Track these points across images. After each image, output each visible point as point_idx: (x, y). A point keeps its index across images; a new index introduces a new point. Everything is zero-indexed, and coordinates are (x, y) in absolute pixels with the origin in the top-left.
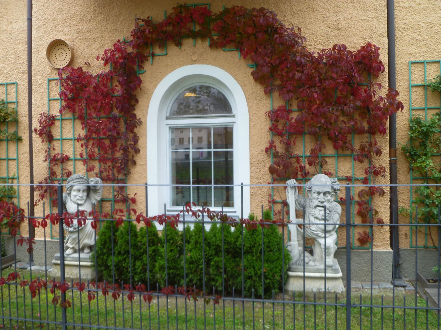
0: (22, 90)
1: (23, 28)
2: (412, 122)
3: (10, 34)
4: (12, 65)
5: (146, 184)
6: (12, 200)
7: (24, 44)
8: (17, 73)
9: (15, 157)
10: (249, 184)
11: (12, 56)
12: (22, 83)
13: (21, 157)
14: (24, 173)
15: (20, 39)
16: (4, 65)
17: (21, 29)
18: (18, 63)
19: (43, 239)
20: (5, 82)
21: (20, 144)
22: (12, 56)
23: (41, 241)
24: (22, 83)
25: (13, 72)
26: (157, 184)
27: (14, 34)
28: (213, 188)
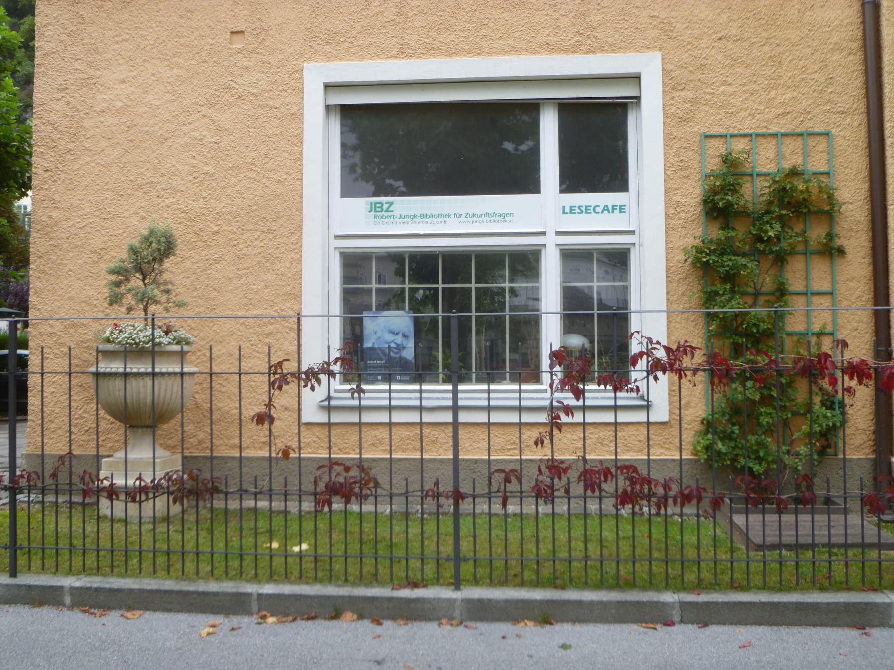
0: (841, 148)
1: (842, 21)
2: (707, 176)
3: (809, 30)
4: (815, 94)
5: (298, 314)
6: (799, 378)
7: (844, 53)
8: (829, 111)
9: (826, 287)
10: (665, 308)
11: (815, 76)
12: (843, 133)
13: (842, 289)
14: (849, 321)
15: (837, 43)
16: (795, 94)
17: (837, 23)
18: (831, 93)
19: (679, 457)
20: (798, 130)
21: (838, 261)
22: (815, 76)
23: (233, 458)
24: (843, 133)
25: (817, 110)
26: (320, 314)
27: (820, 31)
28: (474, 318)
